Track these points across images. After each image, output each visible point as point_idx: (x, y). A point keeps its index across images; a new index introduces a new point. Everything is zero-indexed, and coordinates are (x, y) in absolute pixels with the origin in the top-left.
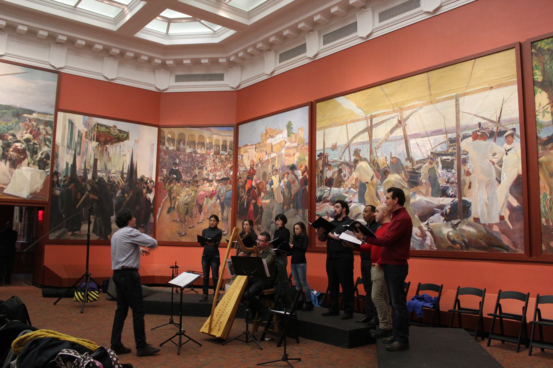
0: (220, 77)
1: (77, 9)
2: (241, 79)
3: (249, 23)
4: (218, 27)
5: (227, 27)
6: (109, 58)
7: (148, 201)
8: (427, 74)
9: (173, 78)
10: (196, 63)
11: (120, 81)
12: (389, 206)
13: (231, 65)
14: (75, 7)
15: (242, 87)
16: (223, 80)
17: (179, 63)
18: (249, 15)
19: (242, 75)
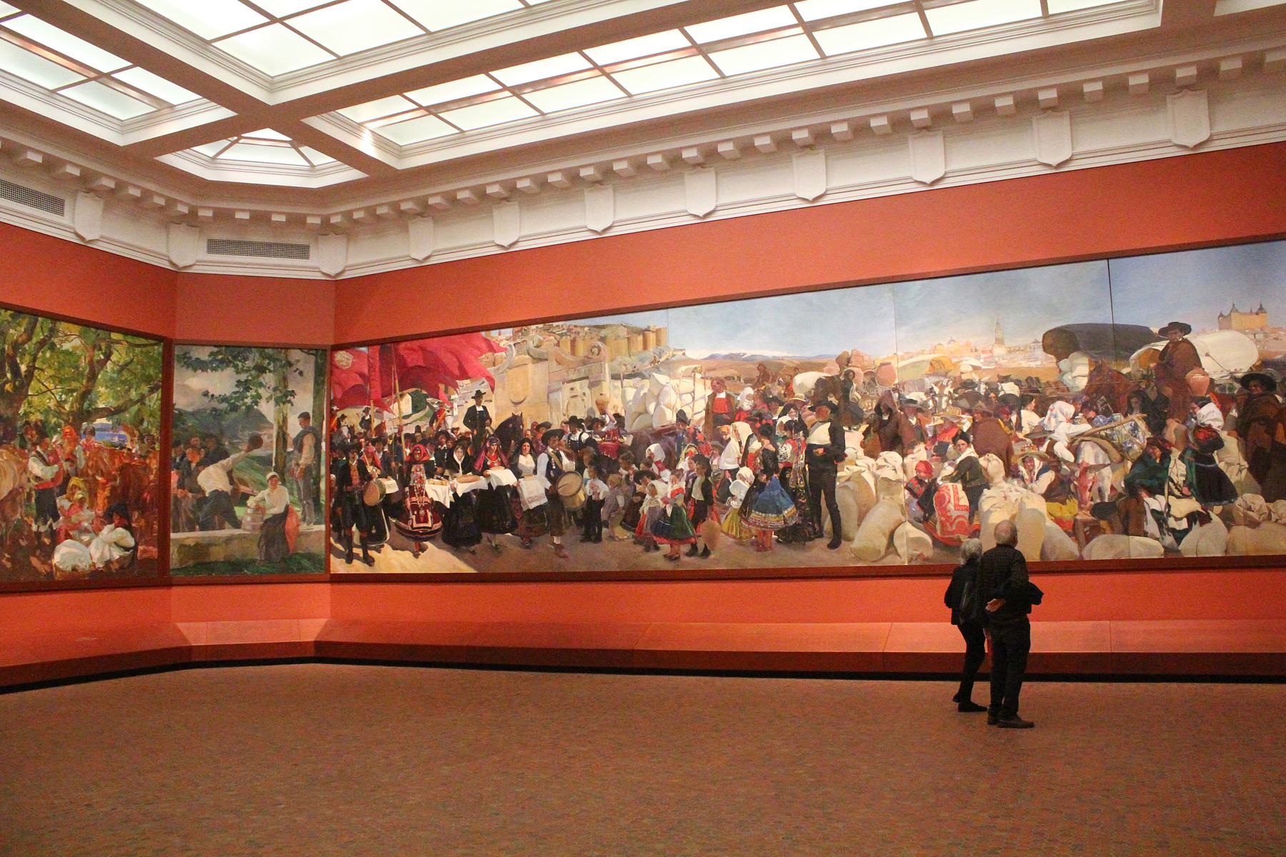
0: (303, 252)
1: (218, 161)
2: (347, 260)
3: (272, 100)
4: (320, 159)
5: (212, 99)
6: (88, 195)
7: (393, 517)
8: (1129, 556)
9: (204, 245)
10: (260, 219)
11: (105, 245)
12: (269, 523)
13: (326, 229)
14: (214, 158)
15: (347, 275)
16: (308, 258)
17: (223, 217)
18: (272, 84)
19: (347, 249)
